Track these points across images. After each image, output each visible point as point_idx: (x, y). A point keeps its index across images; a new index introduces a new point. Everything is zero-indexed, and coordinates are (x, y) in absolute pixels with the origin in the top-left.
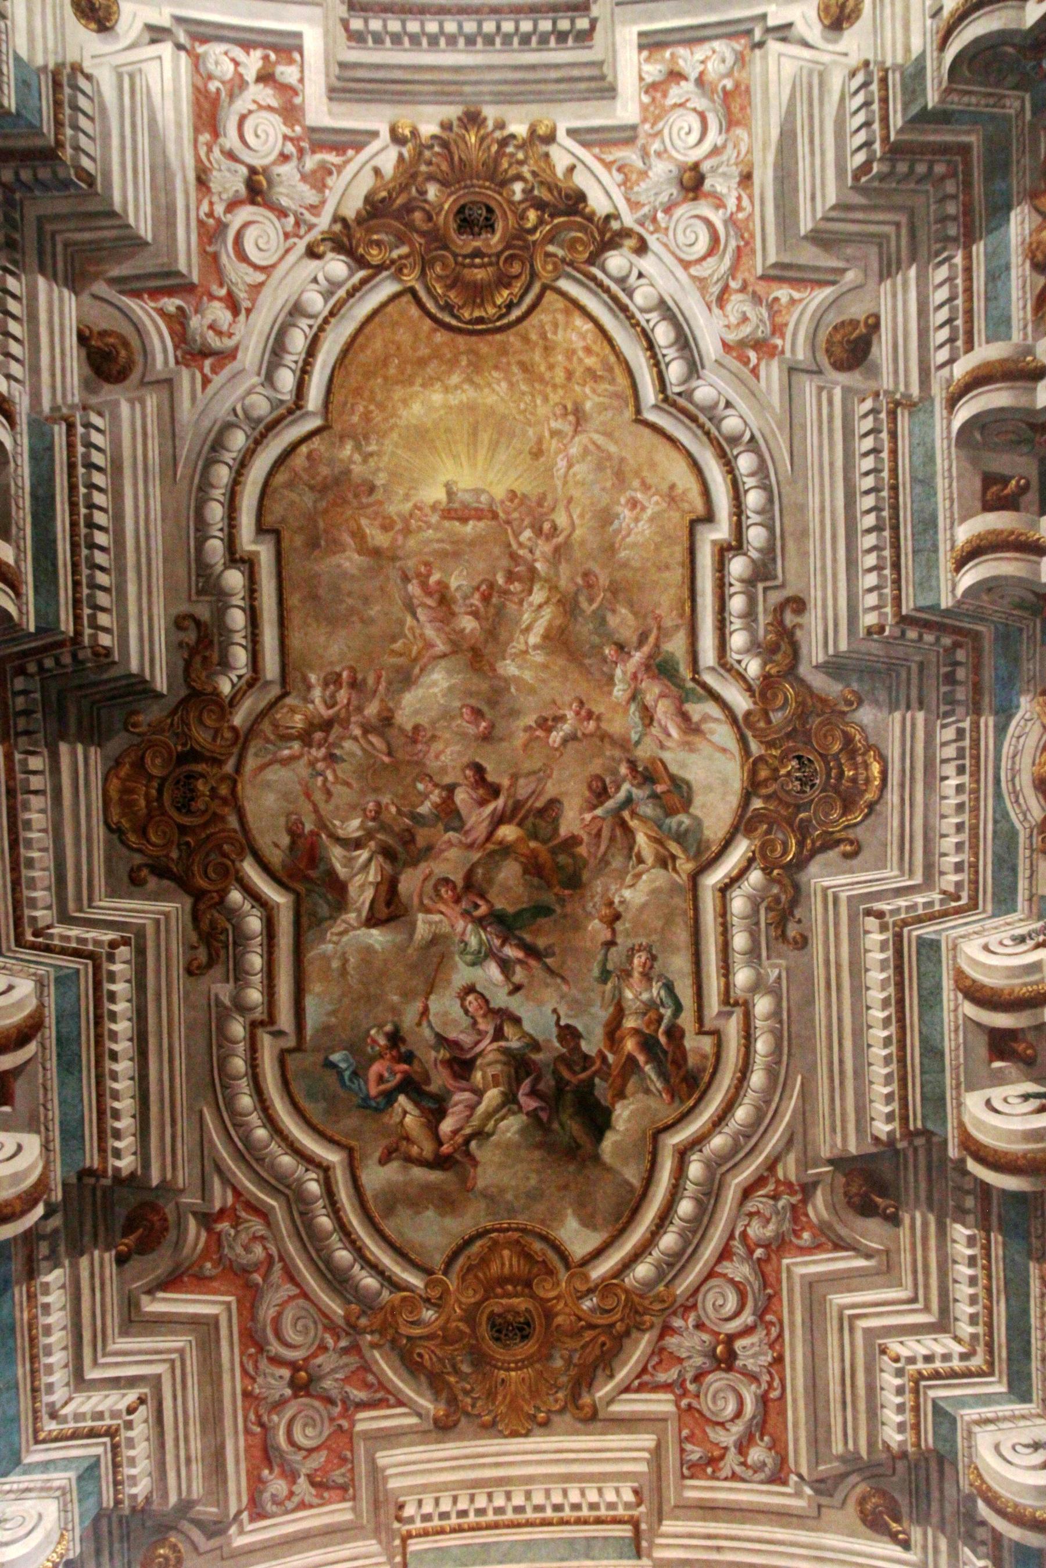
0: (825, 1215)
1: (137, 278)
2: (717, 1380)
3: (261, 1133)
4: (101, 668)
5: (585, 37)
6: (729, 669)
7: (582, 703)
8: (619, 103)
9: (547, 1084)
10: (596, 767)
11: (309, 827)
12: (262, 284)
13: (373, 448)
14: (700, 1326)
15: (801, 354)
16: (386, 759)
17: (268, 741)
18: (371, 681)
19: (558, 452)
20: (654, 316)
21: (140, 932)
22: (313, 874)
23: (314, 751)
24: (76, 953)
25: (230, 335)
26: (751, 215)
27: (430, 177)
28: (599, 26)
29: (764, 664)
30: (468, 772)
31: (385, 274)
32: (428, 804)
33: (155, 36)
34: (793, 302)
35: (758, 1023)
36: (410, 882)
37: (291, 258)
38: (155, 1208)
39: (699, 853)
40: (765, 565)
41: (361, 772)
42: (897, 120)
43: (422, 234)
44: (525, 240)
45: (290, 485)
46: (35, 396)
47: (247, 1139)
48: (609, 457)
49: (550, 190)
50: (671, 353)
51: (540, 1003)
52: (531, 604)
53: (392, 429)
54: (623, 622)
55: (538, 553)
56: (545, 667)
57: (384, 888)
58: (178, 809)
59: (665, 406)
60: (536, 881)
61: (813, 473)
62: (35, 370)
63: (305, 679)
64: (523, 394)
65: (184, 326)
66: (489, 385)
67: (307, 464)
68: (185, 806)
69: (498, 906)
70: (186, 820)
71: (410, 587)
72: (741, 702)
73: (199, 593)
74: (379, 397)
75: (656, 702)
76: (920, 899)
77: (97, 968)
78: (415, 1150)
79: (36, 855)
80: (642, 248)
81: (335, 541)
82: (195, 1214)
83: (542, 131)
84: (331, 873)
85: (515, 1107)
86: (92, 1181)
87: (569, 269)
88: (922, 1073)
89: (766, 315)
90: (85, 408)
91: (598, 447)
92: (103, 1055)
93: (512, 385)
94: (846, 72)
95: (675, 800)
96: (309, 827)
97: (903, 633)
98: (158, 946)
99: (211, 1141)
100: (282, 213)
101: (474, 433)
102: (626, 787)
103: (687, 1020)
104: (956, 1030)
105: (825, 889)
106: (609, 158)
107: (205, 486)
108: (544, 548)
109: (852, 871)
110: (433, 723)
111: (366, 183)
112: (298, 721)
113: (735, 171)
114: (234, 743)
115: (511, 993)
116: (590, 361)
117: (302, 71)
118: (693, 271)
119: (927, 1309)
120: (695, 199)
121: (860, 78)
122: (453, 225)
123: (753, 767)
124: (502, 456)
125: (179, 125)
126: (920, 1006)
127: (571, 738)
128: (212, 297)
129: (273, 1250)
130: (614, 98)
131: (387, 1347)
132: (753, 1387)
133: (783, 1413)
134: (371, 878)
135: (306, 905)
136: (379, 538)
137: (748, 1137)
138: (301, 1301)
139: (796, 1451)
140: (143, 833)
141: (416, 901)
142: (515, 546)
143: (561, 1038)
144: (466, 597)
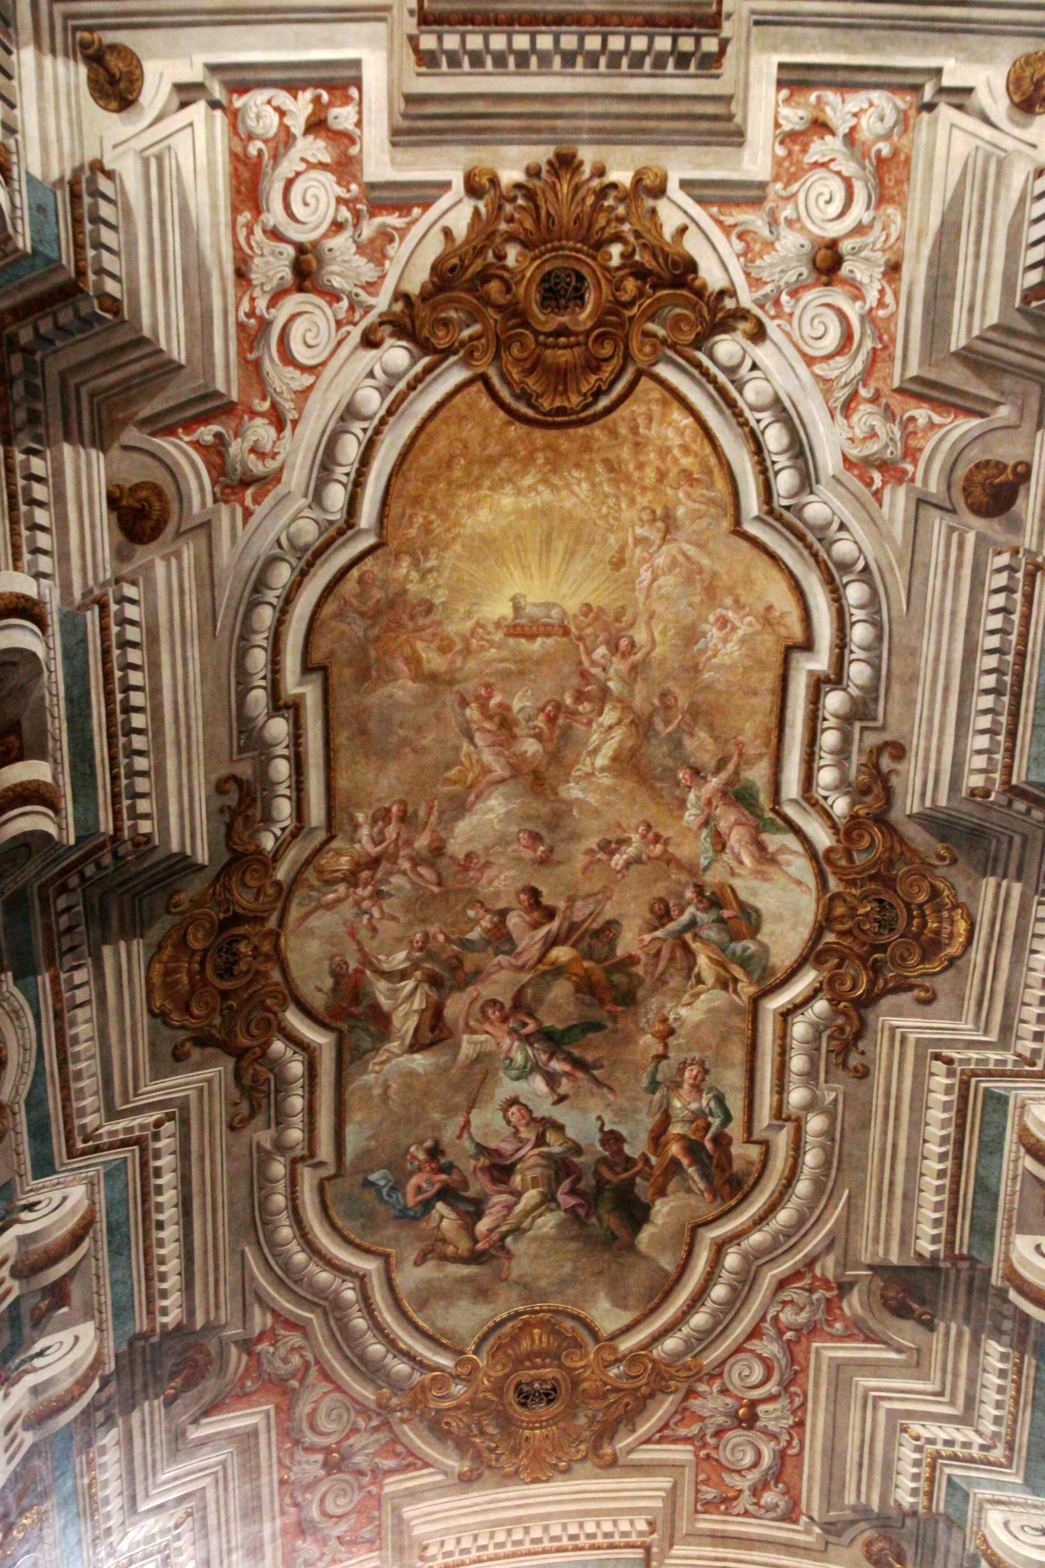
0: (860, 1311)
1: (171, 411)
2: (735, 1437)
3: (300, 1257)
4: (141, 858)
5: (711, 62)
6: (814, 804)
7: (649, 827)
8: (747, 152)
9: (587, 1183)
10: (660, 889)
11: (353, 965)
12: (310, 388)
13: (432, 563)
14: (724, 1391)
15: (934, 487)
16: (436, 889)
17: (311, 887)
18: (422, 813)
19: (643, 561)
20: (766, 417)
21: (184, 1105)
22: (356, 1010)
23: (360, 891)
24: (124, 1143)
25: (274, 456)
26: (894, 315)
27: (511, 238)
28: (730, 50)
29: (853, 804)
30: (523, 897)
31: (452, 359)
32: (478, 929)
33: (185, 97)
34: (932, 426)
35: (809, 1138)
36: (455, 1007)
38: (201, 1349)
39: (762, 979)
40: (865, 704)
41: (409, 907)
43: (499, 308)
44: (618, 314)
45: (340, 615)
46: (66, 588)
47: (286, 1267)
48: (700, 571)
49: (655, 257)
50: (782, 461)
51: (584, 1111)
52: (601, 725)
53: (454, 539)
54: (701, 747)
55: (612, 672)
56: (612, 790)
57: (428, 1014)
58: (221, 977)
59: (769, 519)
60: (587, 998)
61: (931, 616)
62: (64, 557)
63: (352, 818)
64: (606, 496)
65: (222, 455)
66: (568, 486)
67: (358, 589)
68: (227, 972)
69: (547, 1024)
70: (226, 985)
71: (468, 712)
72: (823, 838)
73: (241, 750)
74: (442, 504)
75: (731, 828)
76: (993, 1056)
77: (143, 1151)
78: (450, 1250)
79: (83, 1065)
80: (759, 335)
81: (389, 671)
82: (236, 1343)
84: (375, 1007)
85: (553, 1205)
86: (141, 1343)
87: (670, 353)
88: (974, 1207)
89: (898, 435)
90: (118, 581)
91: (688, 558)
92: (150, 1224)
93: (593, 485)
94: (1031, 168)
95: (744, 928)
96: (353, 965)
97: (1010, 803)
98: (202, 1112)
99: (253, 1278)
100: (333, 296)
101: (547, 542)
102: (691, 910)
103: (736, 1129)
104: (1015, 1178)
105: (893, 1029)
106: (729, 221)
107: (247, 631)
108: (619, 666)
109: (924, 1016)
110: (487, 849)
111: (434, 248)
112: (344, 863)
113: (881, 258)
114: (277, 899)
115: (556, 1103)
116: (686, 462)
117: (360, 112)
118: (818, 369)
119: (952, 1403)
120: (828, 284)
122: (535, 296)
123: (828, 903)
124: (579, 566)
125: (214, 208)
126: (980, 1149)
127: (637, 860)
128: (254, 414)
129: (310, 1357)
130: (741, 145)
131: (417, 1419)
132: (773, 1444)
133: (799, 1467)
134: (416, 1006)
135: (350, 1040)
136: (433, 660)
137: (788, 1236)
138: (336, 1395)
139: (809, 1497)
140: (187, 1010)
141: (461, 1023)
142: (586, 663)
143: (604, 1143)
144: (529, 719)
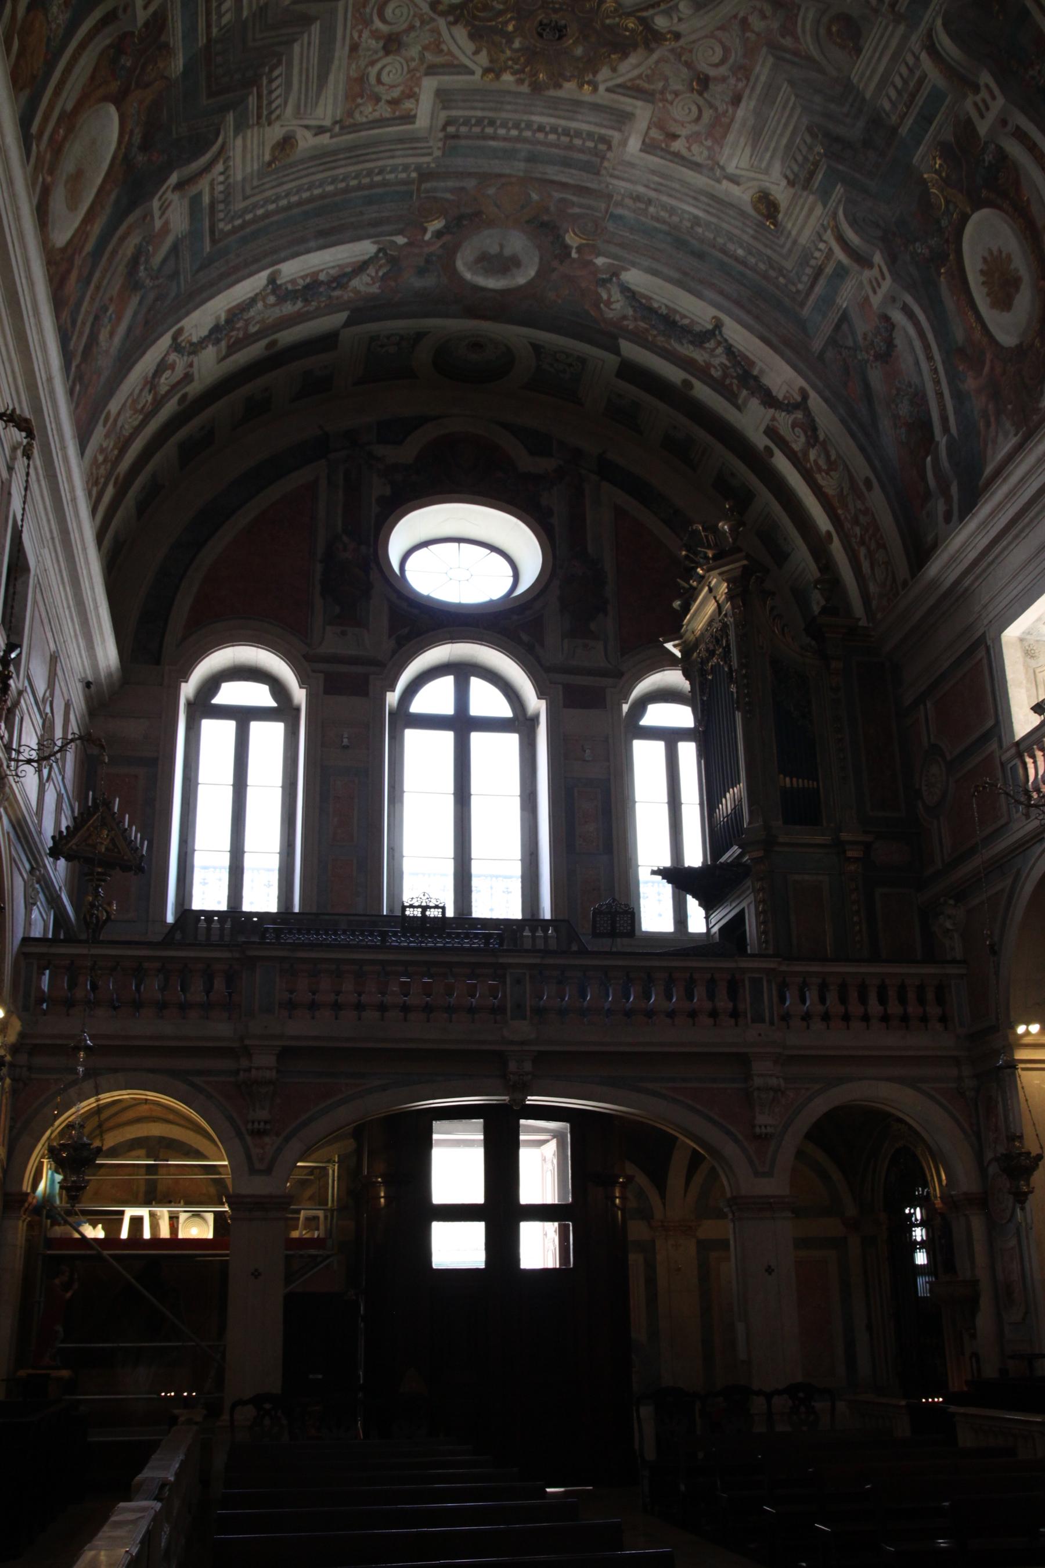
12: (718, 29)
26: (353, 28)
37: (693, 37)
42: (252, 100)
46: (905, 38)
83: (491, 76)
111: (624, 67)
121: (274, 116)
